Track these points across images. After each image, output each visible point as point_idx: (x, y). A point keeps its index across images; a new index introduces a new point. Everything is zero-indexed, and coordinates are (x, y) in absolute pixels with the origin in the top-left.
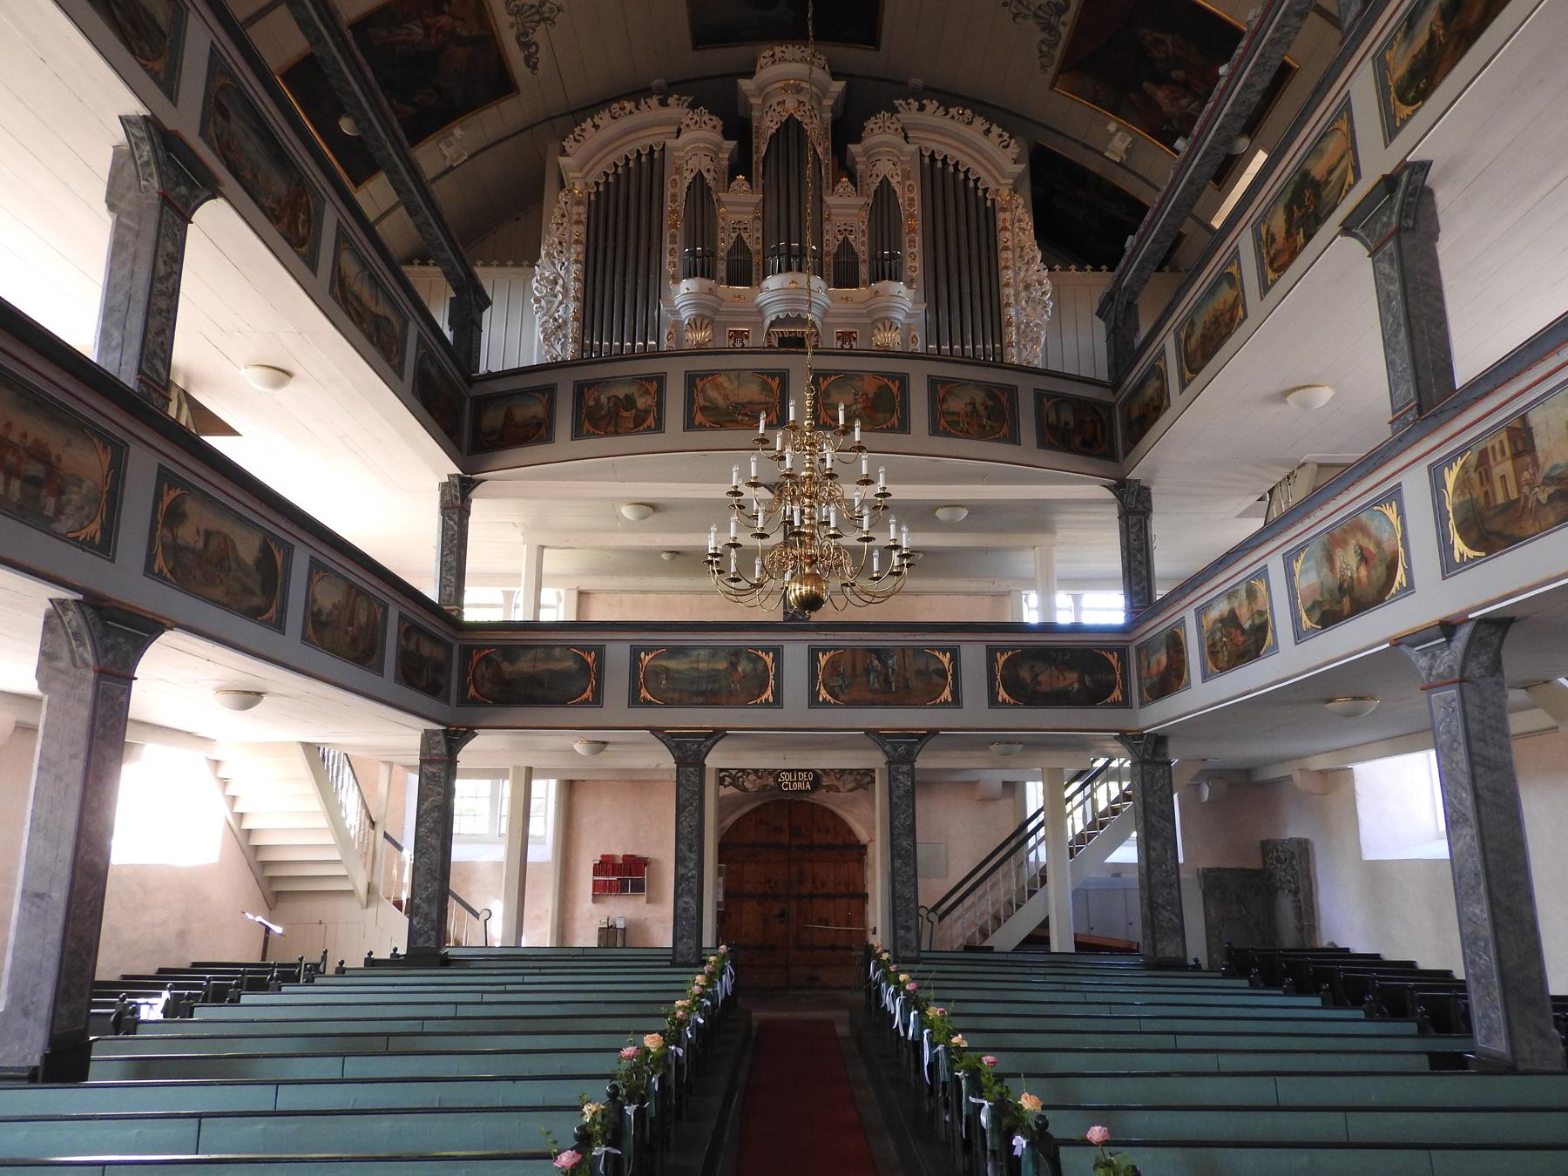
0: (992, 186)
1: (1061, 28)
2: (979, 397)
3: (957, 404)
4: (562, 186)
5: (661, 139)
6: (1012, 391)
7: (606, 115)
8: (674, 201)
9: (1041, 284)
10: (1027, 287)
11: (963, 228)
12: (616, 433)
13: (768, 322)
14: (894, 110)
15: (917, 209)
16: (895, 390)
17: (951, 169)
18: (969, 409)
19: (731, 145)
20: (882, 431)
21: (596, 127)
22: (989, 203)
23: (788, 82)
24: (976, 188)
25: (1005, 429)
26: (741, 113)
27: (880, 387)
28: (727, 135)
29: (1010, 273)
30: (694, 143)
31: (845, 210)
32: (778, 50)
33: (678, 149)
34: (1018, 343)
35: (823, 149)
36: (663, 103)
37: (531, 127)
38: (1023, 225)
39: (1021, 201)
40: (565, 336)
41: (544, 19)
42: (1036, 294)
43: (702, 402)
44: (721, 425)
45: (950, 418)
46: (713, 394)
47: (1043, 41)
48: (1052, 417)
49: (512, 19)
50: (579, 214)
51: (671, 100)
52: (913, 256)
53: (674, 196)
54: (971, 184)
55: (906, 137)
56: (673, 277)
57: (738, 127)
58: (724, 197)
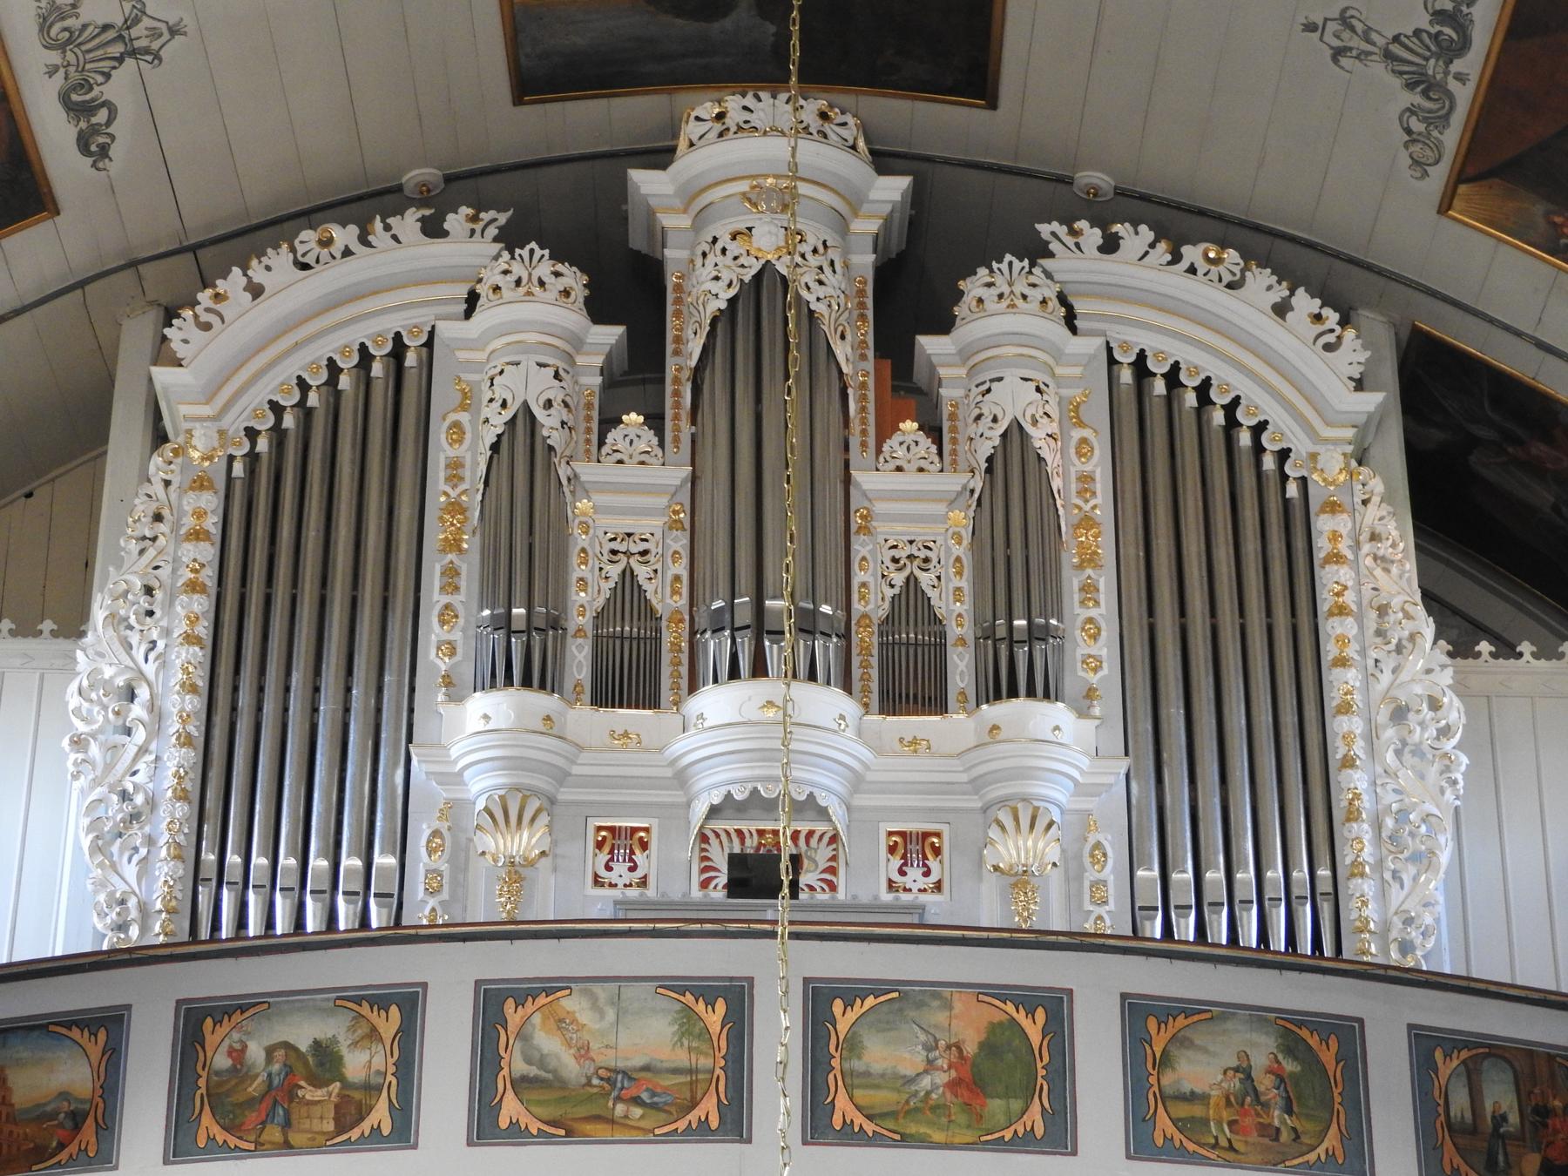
0: (1301, 445)
1: (1453, 85)
2: (1262, 1050)
3: (1201, 1071)
4: (160, 438)
5: (424, 317)
6: (1348, 1033)
7: (281, 259)
8: (454, 478)
9: (1435, 705)
10: (1399, 714)
11: (1223, 554)
12: (287, 1147)
13: (700, 809)
14: (1037, 251)
15: (1101, 504)
16: (1034, 1032)
17: (1191, 399)
18: (1235, 1084)
19: (611, 335)
20: (999, 1145)
21: (256, 291)
22: (1292, 490)
23: (761, 183)
24: (1258, 449)
25: (1331, 1140)
26: (637, 241)
27: (994, 1028)
28: (598, 311)
29: (1352, 676)
30: (519, 333)
31: (912, 508)
32: (733, 103)
33: (470, 345)
34: (1379, 864)
35: (852, 351)
36: (433, 229)
37: (81, 284)
38: (1383, 549)
39: (1377, 485)
40: (150, 841)
41: (133, 53)
42: (1423, 735)
43: (520, 1067)
44: (566, 1129)
45: (1182, 1110)
46: (548, 1042)
47: (1411, 111)
48: (1460, 1102)
49: (54, 57)
50: (200, 514)
51: (455, 222)
52: (1091, 626)
53: (455, 465)
54: (1245, 439)
55: (1070, 320)
56: (448, 681)
57: (628, 286)
58: (587, 471)
